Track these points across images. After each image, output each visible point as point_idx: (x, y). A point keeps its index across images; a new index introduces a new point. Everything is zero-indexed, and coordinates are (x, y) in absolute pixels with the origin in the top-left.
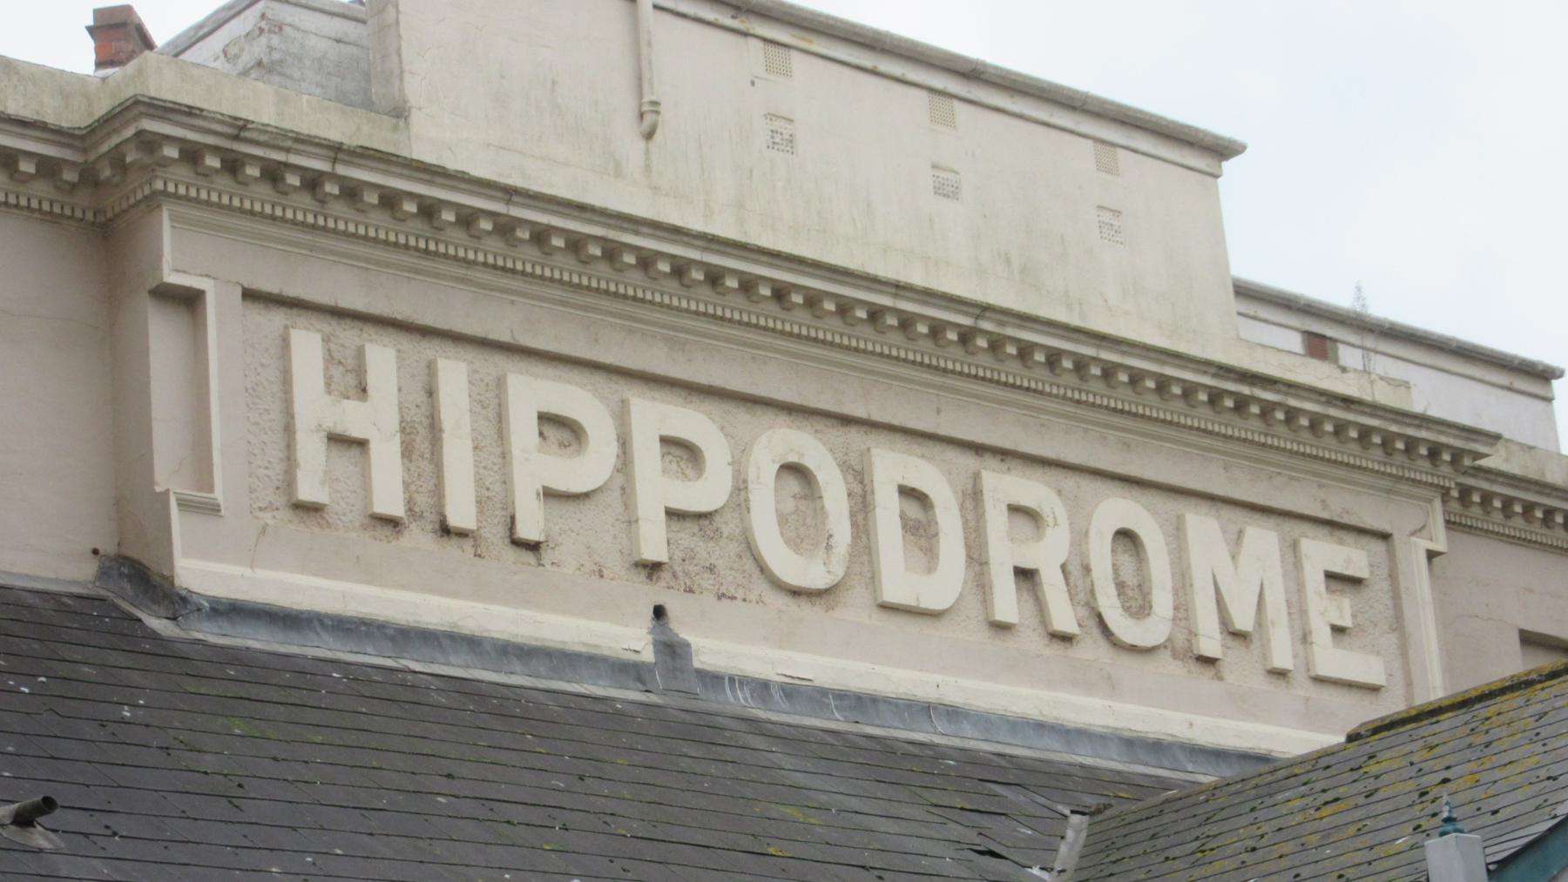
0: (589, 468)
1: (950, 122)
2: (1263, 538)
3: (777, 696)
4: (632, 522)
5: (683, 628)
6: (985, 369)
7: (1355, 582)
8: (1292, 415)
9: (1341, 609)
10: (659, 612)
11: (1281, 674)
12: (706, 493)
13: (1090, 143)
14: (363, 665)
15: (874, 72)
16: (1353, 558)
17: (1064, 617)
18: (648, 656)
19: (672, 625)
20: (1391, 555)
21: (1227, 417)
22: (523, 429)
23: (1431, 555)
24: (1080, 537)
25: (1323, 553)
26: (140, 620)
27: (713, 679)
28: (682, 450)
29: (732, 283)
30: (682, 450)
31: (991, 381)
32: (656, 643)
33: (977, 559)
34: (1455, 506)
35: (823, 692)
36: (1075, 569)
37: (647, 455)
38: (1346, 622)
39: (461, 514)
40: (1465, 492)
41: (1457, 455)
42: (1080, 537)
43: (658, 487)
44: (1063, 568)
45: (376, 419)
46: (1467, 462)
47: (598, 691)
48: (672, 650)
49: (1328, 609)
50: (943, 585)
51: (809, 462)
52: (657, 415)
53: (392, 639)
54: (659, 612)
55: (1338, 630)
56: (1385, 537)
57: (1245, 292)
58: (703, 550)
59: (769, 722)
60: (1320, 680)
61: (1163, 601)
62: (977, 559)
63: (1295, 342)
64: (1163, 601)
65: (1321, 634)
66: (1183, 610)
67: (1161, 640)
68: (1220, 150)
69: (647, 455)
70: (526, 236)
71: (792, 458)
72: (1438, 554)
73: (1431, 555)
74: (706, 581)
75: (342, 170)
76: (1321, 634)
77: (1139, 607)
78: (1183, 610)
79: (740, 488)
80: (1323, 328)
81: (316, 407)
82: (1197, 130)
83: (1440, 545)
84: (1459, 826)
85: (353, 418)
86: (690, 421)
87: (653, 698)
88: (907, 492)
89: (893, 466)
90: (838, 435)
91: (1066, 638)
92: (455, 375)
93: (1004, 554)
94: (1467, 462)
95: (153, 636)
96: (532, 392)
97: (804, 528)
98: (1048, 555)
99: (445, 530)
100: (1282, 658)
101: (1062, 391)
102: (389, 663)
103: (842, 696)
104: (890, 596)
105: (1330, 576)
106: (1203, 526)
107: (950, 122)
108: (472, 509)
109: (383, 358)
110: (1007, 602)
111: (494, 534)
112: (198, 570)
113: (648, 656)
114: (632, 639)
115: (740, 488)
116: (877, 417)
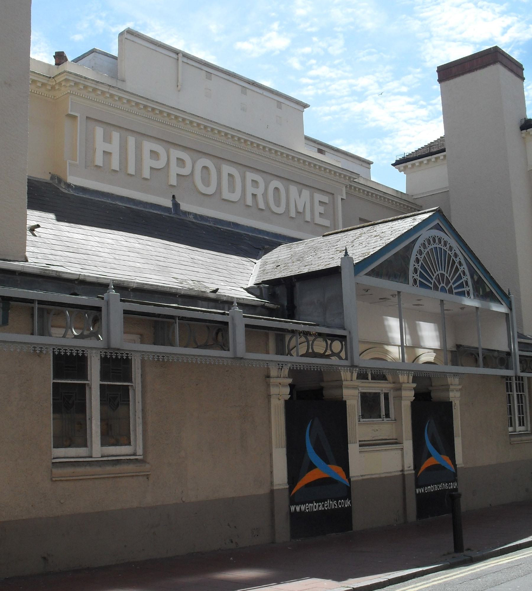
0: (160, 164)
1: (245, 94)
7: (325, 203)
9: (321, 209)
12: (186, 171)
16: (325, 199)
17: (262, 205)
20: (334, 199)
23: (342, 199)
25: (318, 197)
32: (173, 204)
34: (348, 189)
35: (230, 222)
40: (351, 186)
41: (350, 178)
43: (174, 170)
45: (114, 147)
46: (352, 180)
47: (159, 213)
48: (176, 205)
49: (319, 209)
50: (235, 197)
52: (176, 153)
57: (307, 138)
65: (317, 214)
73: (342, 199)
75: (110, 91)
81: (100, 146)
84: (347, 182)
85: (108, 147)
87: (171, 215)
88: (230, 175)
89: (226, 169)
91: (262, 210)
92: (131, 141)
93: (250, 189)
95: (63, 193)
97: (207, 182)
100: (308, 218)
102: (114, 203)
104: (224, 197)
106: (293, 189)
107: (245, 94)
109: (116, 136)
112: (185, 207)
114: (169, 204)
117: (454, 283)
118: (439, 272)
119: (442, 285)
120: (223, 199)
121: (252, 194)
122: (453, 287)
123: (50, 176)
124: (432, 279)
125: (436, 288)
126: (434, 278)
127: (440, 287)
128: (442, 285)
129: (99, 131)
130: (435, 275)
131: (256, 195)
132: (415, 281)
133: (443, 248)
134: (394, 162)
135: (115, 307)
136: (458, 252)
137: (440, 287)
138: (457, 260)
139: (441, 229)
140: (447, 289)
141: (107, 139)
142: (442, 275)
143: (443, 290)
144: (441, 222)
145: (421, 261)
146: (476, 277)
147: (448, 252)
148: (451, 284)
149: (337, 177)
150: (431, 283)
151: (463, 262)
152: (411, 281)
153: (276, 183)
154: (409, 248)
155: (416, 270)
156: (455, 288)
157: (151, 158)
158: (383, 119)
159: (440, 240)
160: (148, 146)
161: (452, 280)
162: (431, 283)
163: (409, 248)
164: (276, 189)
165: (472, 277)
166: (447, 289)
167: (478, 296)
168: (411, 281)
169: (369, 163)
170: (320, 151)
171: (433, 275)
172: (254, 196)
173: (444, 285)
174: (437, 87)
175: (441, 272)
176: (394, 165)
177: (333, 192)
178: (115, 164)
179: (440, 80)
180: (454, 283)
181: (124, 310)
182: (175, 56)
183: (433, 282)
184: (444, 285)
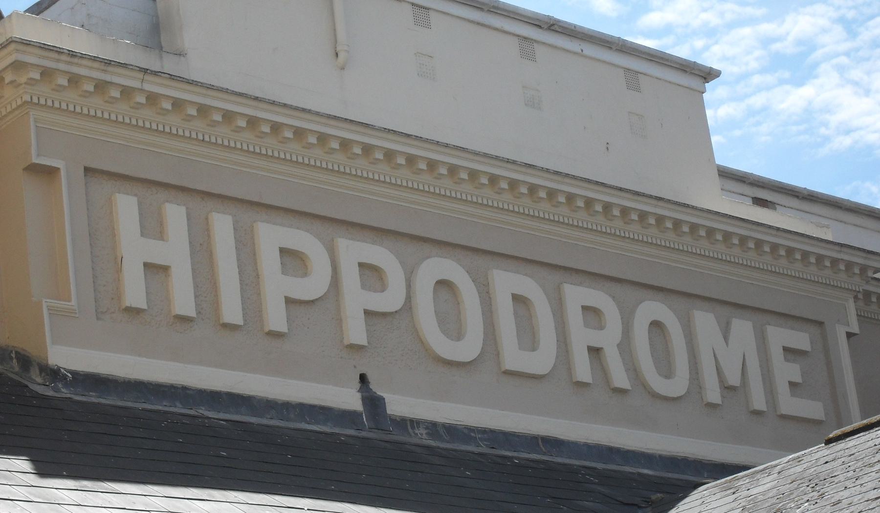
0: (313, 286)
2: (743, 328)
4: (339, 321)
6: (799, 272)
10: (363, 378)
11: (757, 413)
12: (390, 300)
13: (516, 39)
14: (311, 431)
15: (581, 54)
16: (801, 340)
17: (620, 378)
19: (371, 387)
22: (269, 261)
23: (849, 335)
26: (27, 386)
27: (405, 424)
28: (292, 259)
31: (568, 224)
32: (364, 400)
34: (861, 304)
37: (351, 278)
38: (798, 379)
43: (356, 299)
48: (374, 403)
49: (791, 371)
50: (541, 361)
52: (354, 251)
54: (363, 378)
55: (792, 384)
56: (820, 324)
59: (438, 448)
60: (783, 417)
65: (783, 389)
67: (682, 393)
68: (708, 75)
69: (351, 278)
72: (855, 334)
73: (849, 335)
76: (783, 389)
81: (134, 250)
82: (575, 26)
83: (855, 329)
85: (157, 252)
86: (378, 254)
87: (364, 434)
92: (222, 225)
93: (581, 337)
94: (870, 274)
96: (271, 236)
98: (608, 339)
100: (759, 402)
101: (613, 231)
102: (192, 412)
103: (662, 458)
105: (786, 349)
108: (364, 335)
109: (175, 215)
114: (349, 399)
115: (409, 298)
120: (508, 373)
129: (126, 207)
141: (153, 227)
149: (783, 262)
153: (652, 309)
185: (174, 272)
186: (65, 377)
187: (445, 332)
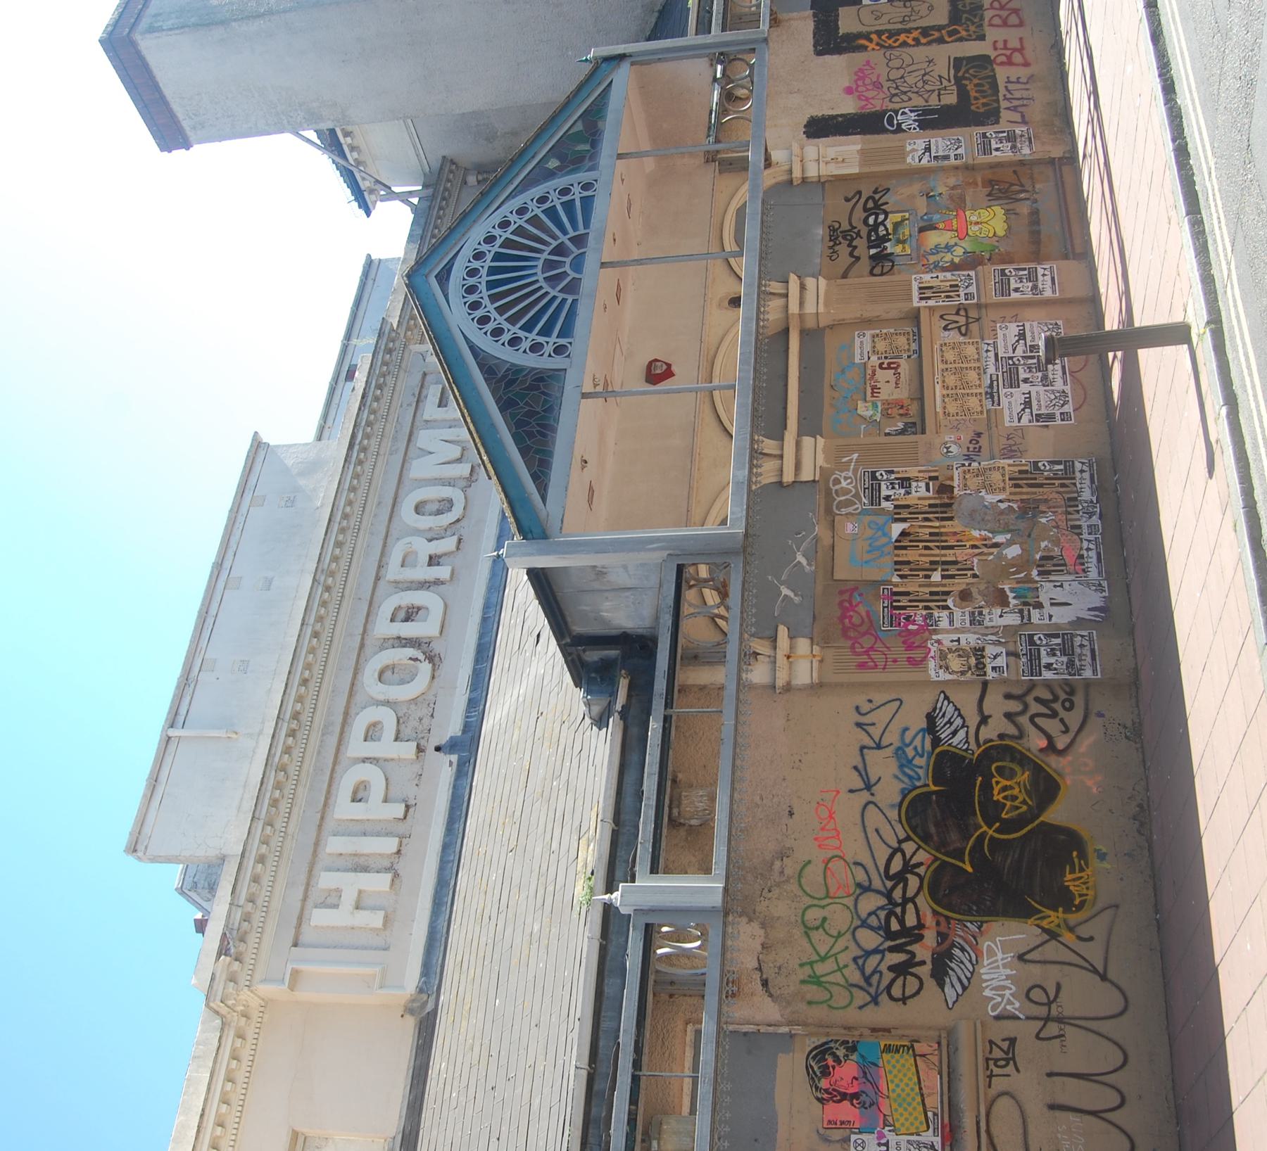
1: (264, 498)
2: (424, 438)
3: (474, 695)
5: (443, 740)
8: (369, 424)
10: (438, 749)
12: (388, 719)
18: (454, 758)
21: (369, 456)
24: (417, 532)
28: (372, 733)
29: (341, 537)
30: (372, 733)
33: (424, 585)
35: (474, 670)
36: (429, 536)
39: (390, 845)
42: (417, 532)
43: (386, 747)
44: (430, 540)
45: (351, 884)
51: (379, 667)
52: (356, 746)
53: (442, 887)
54: (438, 749)
56: (425, 374)
57: (319, 438)
58: (413, 723)
61: (446, 492)
62: (424, 585)
63: (349, 385)
64: (446, 492)
66: (450, 483)
68: (257, 445)
69: (371, 749)
70: (331, 579)
71: (376, 675)
74: (426, 721)
77: (448, 504)
78: (450, 483)
79: (387, 703)
80: (344, 372)
85: (348, 899)
90: (368, 650)
92: (335, 845)
93: (423, 572)
98: (425, 549)
99: (399, 852)
109: (326, 880)
110: (443, 572)
111: (402, 828)
113: (454, 758)
115: (387, 703)
116: (392, 495)
117: (565, 232)
118: (540, 277)
119: (567, 268)
120: (441, 633)
121: (430, 565)
122: (572, 234)
123: (408, 1017)
124: (554, 298)
125: (573, 287)
126: (553, 293)
127: (572, 275)
128: (567, 268)
129: (319, 918)
130: (546, 288)
131: (431, 557)
132: (559, 350)
133: (488, 263)
134: (362, 212)
135: (646, 889)
136: (497, 218)
137: (572, 275)
138: (502, 235)
139: (448, 270)
140: (576, 252)
141: (331, 901)
142: (549, 265)
143: (578, 265)
144: (430, 271)
145: (533, 336)
146: (553, 163)
147: (496, 249)
148: (564, 239)
149: (397, 344)
150: (564, 300)
151: (516, 203)
152: (557, 362)
153: (406, 511)
154: (489, 367)
155: (536, 348)
156: (575, 228)
157: (379, 740)
158: (270, 270)
159: (471, 290)
160: (344, 809)
161: (554, 237)
162: (564, 300)
163: (489, 367)
164: (419, 509)
165: (551, 175)
166: (576, 252)
167: (591, 158)
168: (557, 362)
169: (369, 264)
170: (350, 376)
171: (547, 293)
172: (433, 561)
173: (568, 260)
174: (202, 153)
175: (539, 270)
176: (368, 213)
177: (419, 376)
178: (379, 883)
179: (187, 146)
180: (565, 232)
181: (651, 872)
182: (172, 747)
183: (561, 296)
184: (568, 260)
185: (432, 552)
186: (425, 982)
187: (450, 509)
